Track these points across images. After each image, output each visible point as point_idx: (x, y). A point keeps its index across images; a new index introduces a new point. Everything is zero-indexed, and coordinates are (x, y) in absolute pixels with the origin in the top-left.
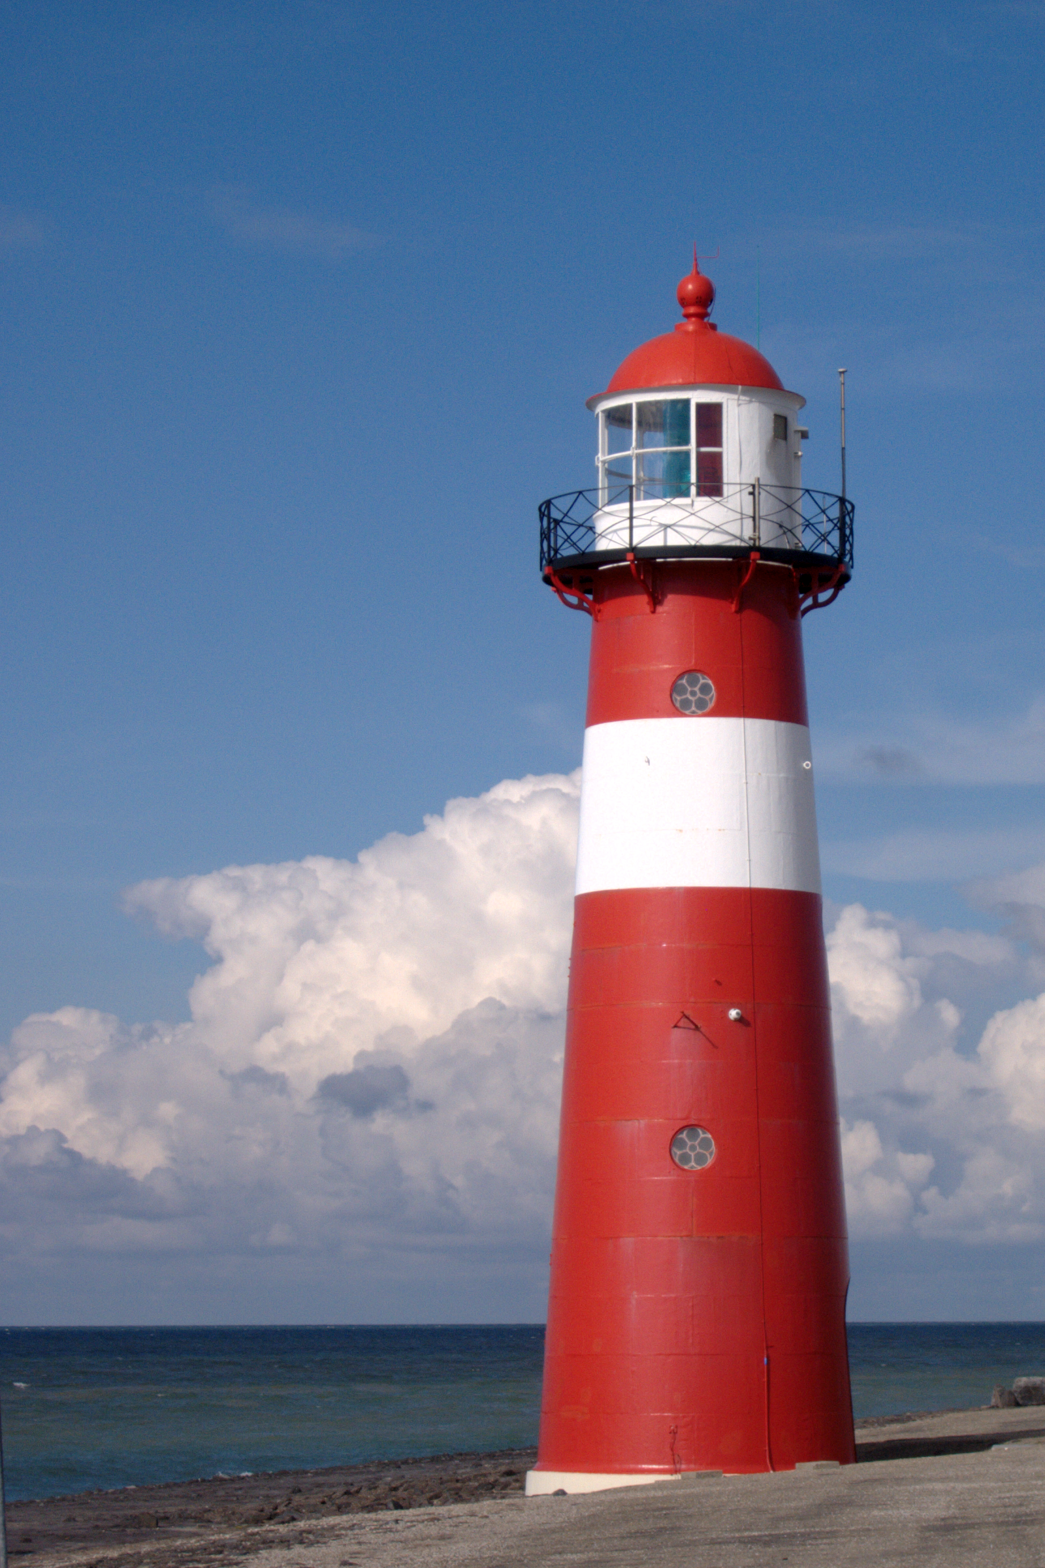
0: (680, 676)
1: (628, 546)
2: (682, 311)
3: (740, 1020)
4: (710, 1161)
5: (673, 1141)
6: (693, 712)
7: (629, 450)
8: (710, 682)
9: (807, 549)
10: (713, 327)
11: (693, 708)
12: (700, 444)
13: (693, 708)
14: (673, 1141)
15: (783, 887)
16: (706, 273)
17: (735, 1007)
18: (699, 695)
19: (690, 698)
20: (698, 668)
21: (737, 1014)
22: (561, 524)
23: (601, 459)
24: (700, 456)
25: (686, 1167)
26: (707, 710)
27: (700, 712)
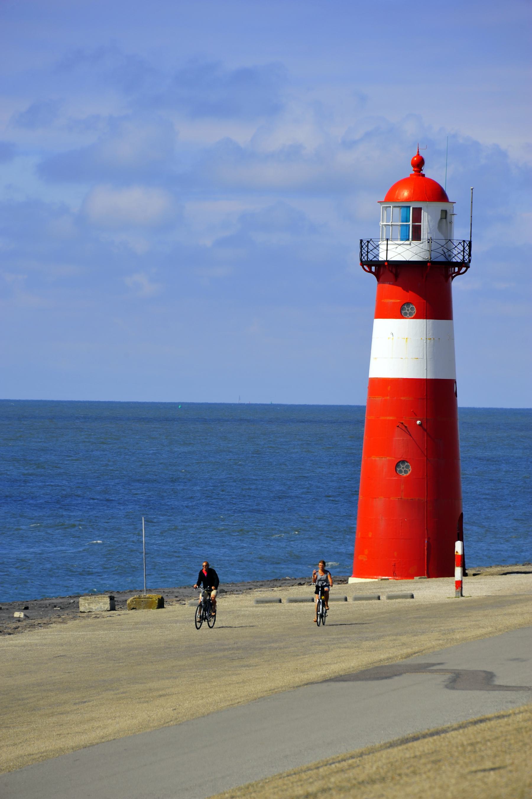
0: (404, 304)
1: (386, 260)
2: (413, 168)
3: (420, 425)
4: (409, 473)
5: (397, 465)
6: (408, 317)
7: (389, 223)
8: (414, 307)
9: (449, 260)
10: (423, 175)
11: (408, 316)
12: (413, 222)
13: (408, 316)
14: (397, 465)
15: (434, 378)
16: (421, 154)
17: (419, 420)
18: (410, 311)
19: (407, 312)
20: (410, 302)
21: (419, 423)
22: (370, 242)
23: (381, 224)
24: (413, 226)
25: (401, 474)
26: (412, 317)
27: (410, 317)
